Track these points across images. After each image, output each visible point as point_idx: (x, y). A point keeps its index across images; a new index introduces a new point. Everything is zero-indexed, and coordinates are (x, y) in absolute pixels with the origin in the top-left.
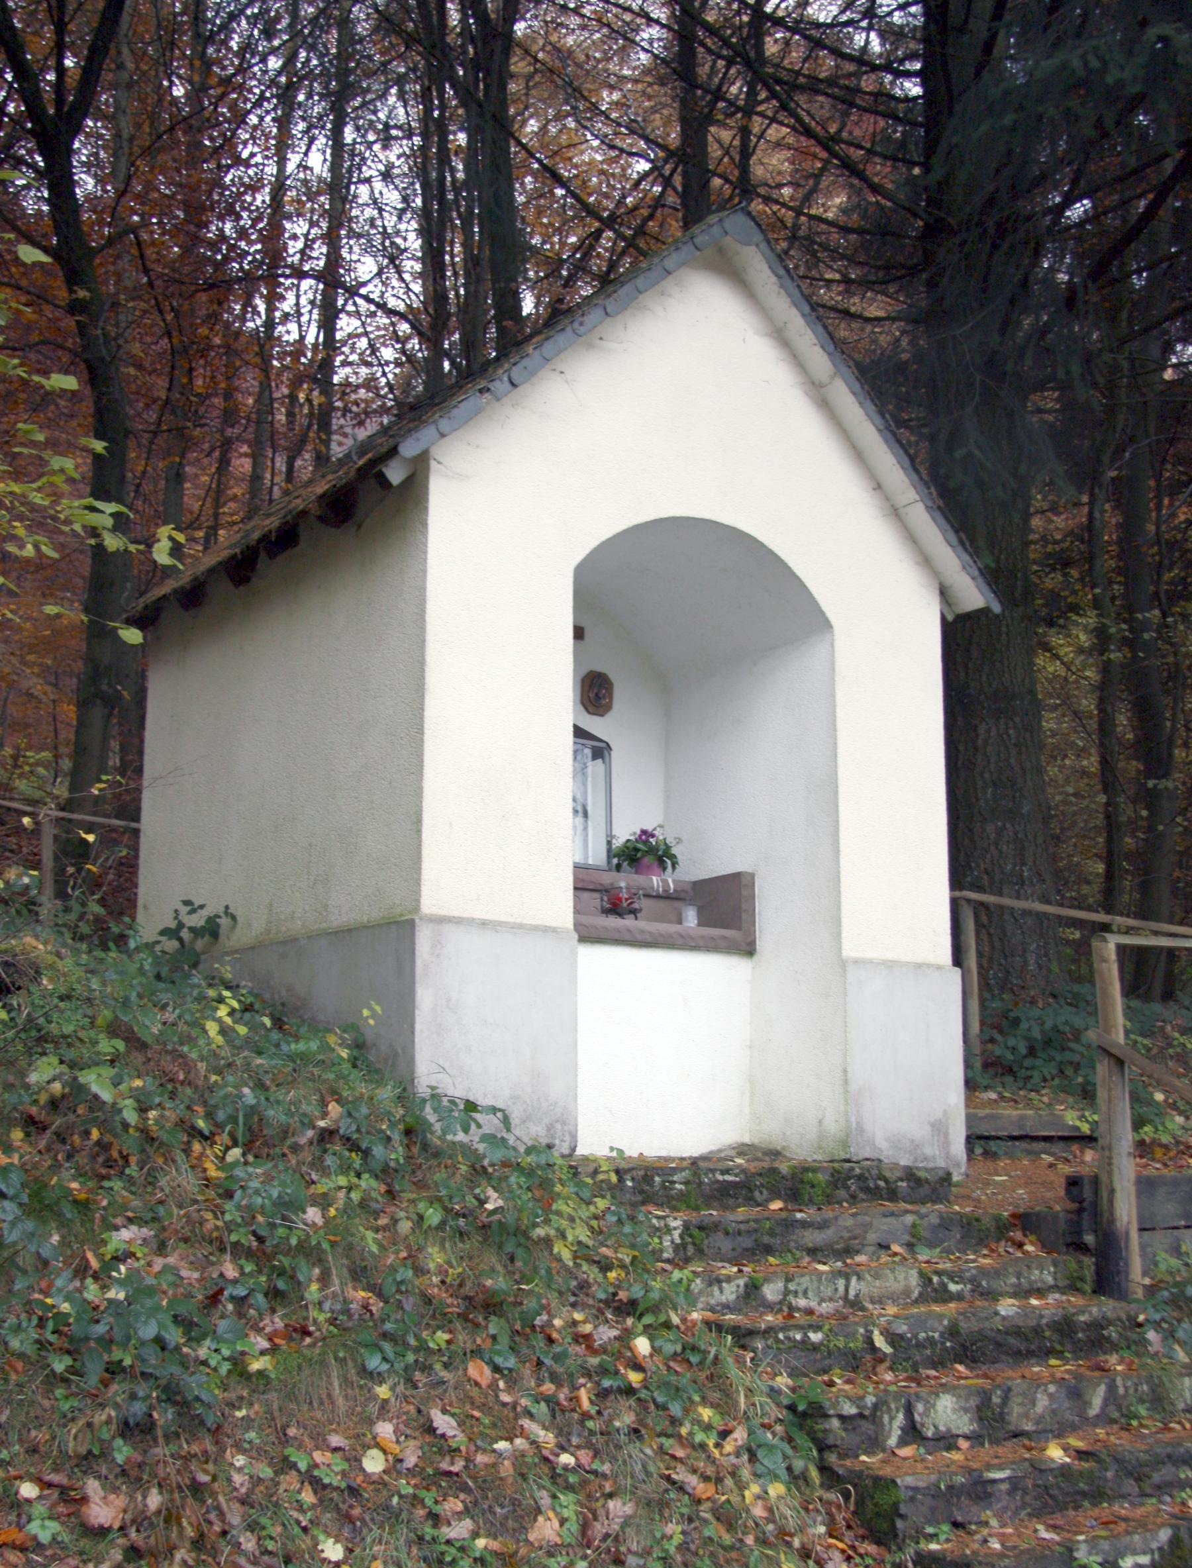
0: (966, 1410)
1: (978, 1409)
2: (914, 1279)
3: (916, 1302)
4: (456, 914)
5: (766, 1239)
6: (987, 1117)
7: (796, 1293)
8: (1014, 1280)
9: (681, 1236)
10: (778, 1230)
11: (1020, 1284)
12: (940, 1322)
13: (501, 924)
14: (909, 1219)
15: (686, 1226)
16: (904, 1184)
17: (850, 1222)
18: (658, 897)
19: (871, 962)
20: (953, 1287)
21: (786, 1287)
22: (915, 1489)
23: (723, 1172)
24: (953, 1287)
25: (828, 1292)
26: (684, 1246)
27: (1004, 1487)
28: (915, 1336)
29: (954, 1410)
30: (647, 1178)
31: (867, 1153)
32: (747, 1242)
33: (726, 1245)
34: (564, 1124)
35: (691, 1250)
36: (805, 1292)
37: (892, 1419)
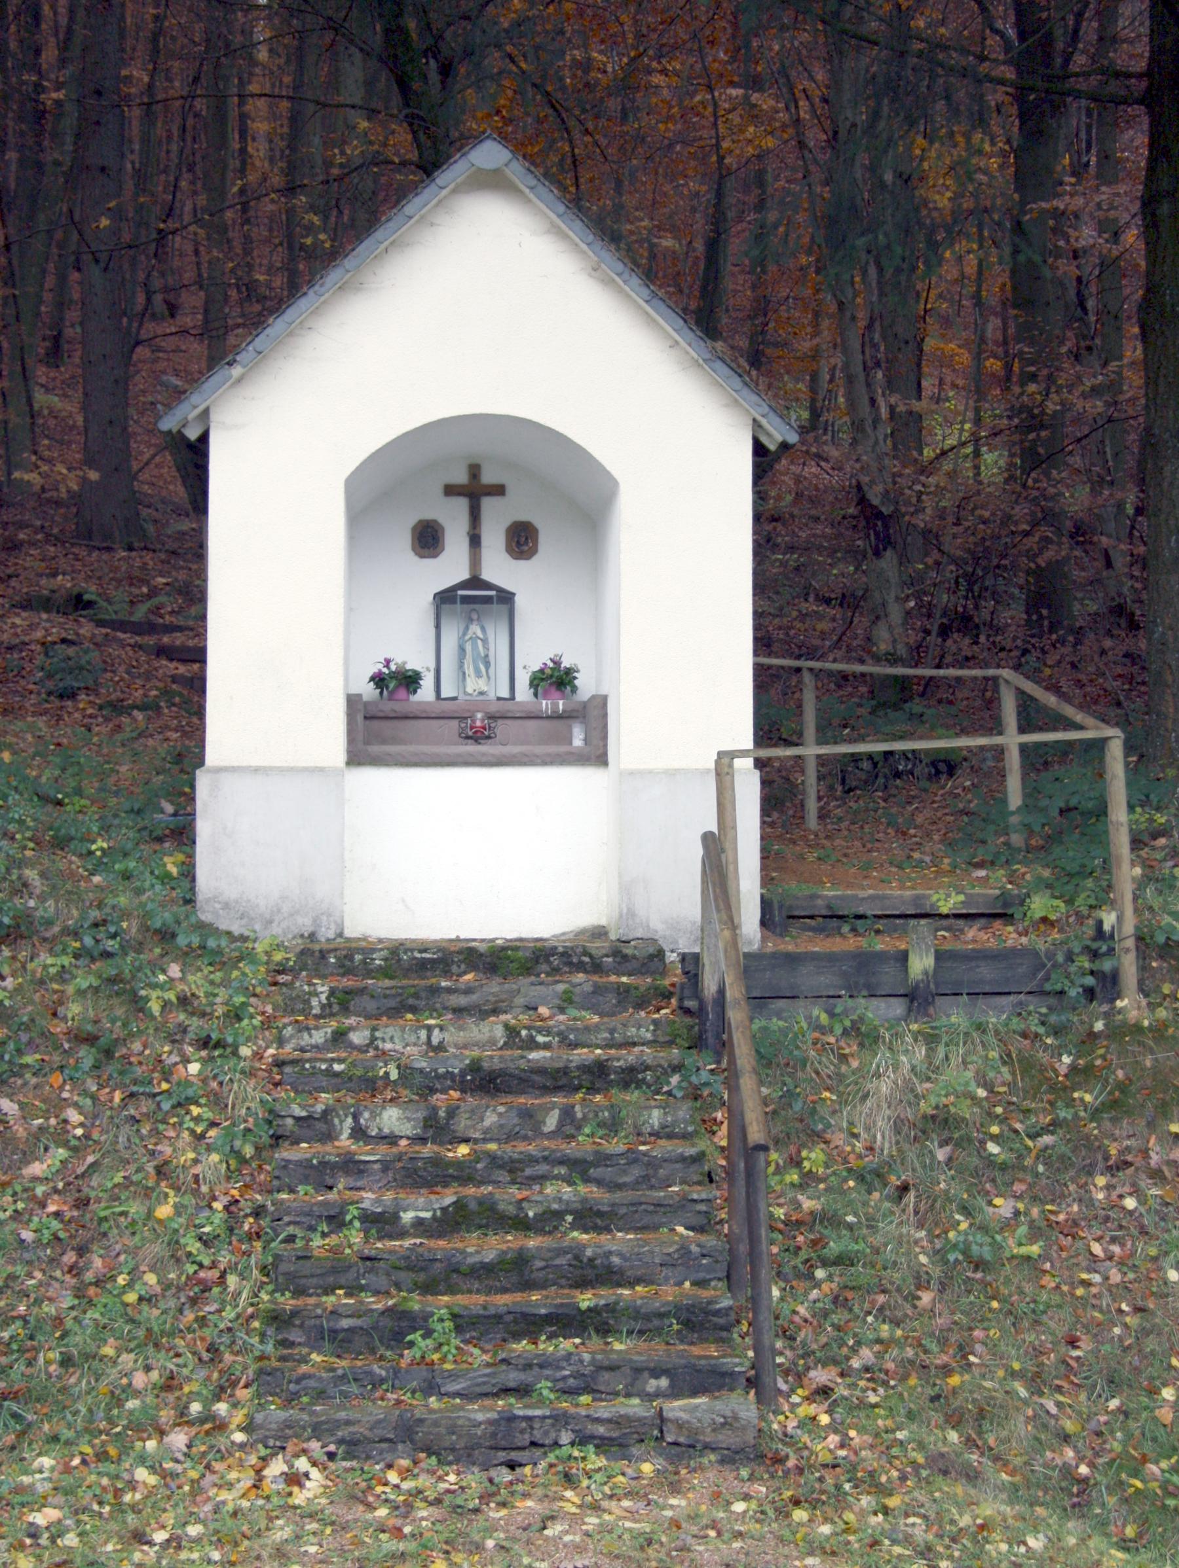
0: (409, 1119)
1: (426, 1120)
2: (499, 1033)
3: (501, 1049)
4: (236, 764)
5: (411, 1001)
6: (871, 897)
7: (383, 1040)
8: (607, 1035)
9: (328, 998)
10: (423, 994)
11: (613, 1038)
12: (462, 1061)
13: (271, 769)
14: (561, 987)
15: (332, 992)
16: (610, 959)
17: (496, 989)
18: (548, 717)
19: (650, 772)
20: (540, 1039)
21: (372, 1035)
22: (288, 1161)
23: (421, 951)
24: (540, 1039)
25: (413, 1039)
26: (330, 1005)
27: (377, 1166)
28: (436, 1070)
29: (399, 1119)
30: (349, 957)
31: (639, 933)
32: (392, 1003)
33: (371, 1006)
34: (329, 915)
35: (336, 1008)
36: (392, 1038)
37: (341, 1122)
